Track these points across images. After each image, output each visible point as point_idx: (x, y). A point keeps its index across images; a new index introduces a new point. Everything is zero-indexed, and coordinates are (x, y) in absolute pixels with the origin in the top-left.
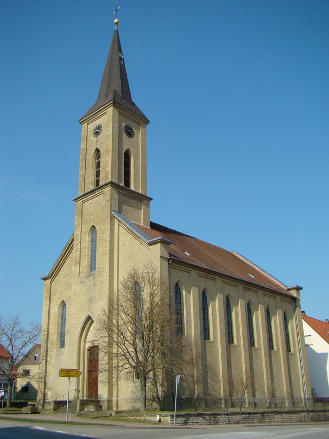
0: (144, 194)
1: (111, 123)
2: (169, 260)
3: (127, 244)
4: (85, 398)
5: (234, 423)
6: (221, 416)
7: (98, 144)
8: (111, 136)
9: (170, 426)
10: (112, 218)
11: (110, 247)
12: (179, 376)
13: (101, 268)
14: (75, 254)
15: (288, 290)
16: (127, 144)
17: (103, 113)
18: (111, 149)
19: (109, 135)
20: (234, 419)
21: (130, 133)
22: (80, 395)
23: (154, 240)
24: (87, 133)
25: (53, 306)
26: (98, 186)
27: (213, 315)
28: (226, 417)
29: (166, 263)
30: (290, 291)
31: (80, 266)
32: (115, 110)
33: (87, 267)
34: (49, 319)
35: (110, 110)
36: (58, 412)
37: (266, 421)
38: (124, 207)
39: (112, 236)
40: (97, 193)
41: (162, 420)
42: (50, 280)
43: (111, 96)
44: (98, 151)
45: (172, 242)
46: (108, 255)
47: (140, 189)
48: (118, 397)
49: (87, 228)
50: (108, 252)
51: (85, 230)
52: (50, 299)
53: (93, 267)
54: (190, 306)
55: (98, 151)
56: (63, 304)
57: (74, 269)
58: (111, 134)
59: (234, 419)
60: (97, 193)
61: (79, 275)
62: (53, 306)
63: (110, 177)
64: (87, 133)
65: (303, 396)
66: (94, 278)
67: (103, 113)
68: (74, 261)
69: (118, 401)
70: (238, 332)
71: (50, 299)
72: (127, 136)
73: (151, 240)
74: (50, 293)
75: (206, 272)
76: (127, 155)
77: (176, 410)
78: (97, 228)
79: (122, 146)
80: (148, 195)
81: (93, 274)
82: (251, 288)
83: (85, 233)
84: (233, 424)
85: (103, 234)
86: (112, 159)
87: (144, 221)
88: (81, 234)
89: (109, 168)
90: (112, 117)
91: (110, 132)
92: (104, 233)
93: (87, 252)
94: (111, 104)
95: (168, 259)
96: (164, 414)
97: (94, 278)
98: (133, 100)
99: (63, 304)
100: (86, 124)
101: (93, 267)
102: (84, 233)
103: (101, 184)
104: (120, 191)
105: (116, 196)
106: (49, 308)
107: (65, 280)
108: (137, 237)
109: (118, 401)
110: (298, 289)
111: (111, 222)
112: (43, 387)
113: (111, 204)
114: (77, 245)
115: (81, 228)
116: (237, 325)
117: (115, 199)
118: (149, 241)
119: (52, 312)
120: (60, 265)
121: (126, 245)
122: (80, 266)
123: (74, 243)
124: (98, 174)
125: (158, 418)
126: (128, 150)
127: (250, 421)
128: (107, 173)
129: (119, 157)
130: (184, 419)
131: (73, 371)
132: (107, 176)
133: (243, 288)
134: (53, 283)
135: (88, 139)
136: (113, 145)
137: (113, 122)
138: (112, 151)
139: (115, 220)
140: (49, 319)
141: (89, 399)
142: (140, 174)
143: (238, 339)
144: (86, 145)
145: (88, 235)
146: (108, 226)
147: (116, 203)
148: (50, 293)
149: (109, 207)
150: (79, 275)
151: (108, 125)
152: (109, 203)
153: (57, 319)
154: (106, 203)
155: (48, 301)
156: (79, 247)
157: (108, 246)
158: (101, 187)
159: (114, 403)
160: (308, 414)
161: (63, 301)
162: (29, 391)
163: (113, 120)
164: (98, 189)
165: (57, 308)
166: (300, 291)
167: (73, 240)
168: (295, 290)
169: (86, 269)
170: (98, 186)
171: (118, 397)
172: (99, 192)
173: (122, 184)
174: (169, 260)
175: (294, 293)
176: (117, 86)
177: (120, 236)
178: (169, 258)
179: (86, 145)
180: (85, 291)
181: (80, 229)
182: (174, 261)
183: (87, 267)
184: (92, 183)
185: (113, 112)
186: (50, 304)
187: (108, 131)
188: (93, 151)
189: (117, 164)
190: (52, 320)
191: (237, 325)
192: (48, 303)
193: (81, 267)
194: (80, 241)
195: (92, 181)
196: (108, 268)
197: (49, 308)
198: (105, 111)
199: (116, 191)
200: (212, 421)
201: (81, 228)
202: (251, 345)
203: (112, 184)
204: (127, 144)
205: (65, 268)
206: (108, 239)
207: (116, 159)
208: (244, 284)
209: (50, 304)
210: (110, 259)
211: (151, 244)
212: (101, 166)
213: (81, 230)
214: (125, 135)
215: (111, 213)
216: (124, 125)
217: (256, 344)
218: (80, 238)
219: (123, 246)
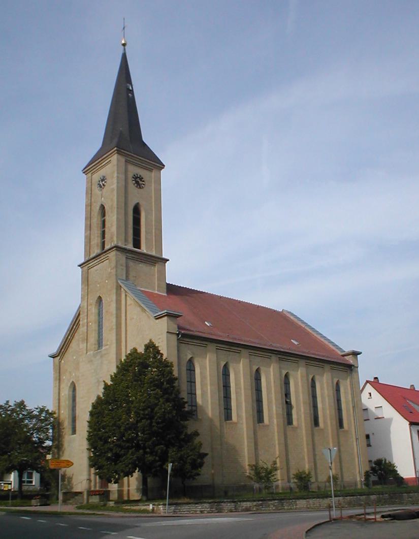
0: (158, 255)
1: (115, 175)
2: (178, 335)
3: (135, 317)
4: (97, 489)
5: (243, 511)
6: (225, 504)
7: (103, 199)
8: (116, 190)
9: (162, 514)
10: (119, 288)
11: (117, 321)
12: (171, 464)
13: (107, 345)
14: (82, 329)
15: (343, 356)
17: (107, 161)
18: (116, 206)
19: (113, 189)
20: (242, 507)
21: (138, 181)
22: (92, 484)
23: (160, 313)
24: (91, 185)
25: (63, 388)
26: (104, 251)
27: (237, 393)
28: (233, 504)
29: (174, 338)
30: (346, 357)
31: (87, 342)
33: (95, 344)
34: (59, 403)
35: (115, 158)
37: (286, 507)
39: (118, 309)
40: (102, 258)
41: (155, 509)
42: (59, 357)
43: (115, 141)
44: (103, 208)
45: (181, 314)
46: (115, 330)
47: (154, 249)
48: (129, 486)
50: (115, 327)
51: (91, 301)
52: (60, 380)
53: (100, 344)
54: (207, 384)
55: (103, 208)
56: (73, 387)
57: (81, 346)
58: (116, 188)
59: (242, 507)
60: (102, 258)
61: (87, 353)
62: (63, 388)
63: (115, 239)
64: (91, 185)
65: (358, 479)
67: (107, 161)
68: (81, 336)
69: (129, 490)
70: (270, 410)
71: (60, 380)
72: (137, 187)
73: (157, 314)
74: (60, 373)
75: (227, 345)
76: (137, 210)
77: (169, 498)
78: (103, 299)
80: (164, 256)
81: (100, 352)
82: (289, 358)
83: (91, 305)
84: (242, 511)
85: (110, 306)
86: (117, 218)
87: (158, 287)
89: (114, 229)
91: (115, 186)
92: (110, 305)
93: (94, 326)
94: (115, 151)
95: (177, 334)
96: (156, 503)
99: (73, 387)
100: (90, 174)
101: (100, 344)
103: (107, 247)
104: (128, 254)
106: (59, 389)
107: (74, 358)
108: (144, 310)
109: (129, 490)
110: (355, 354)
111: (116, 293)
114: (83, 319)
115: (88, 298)
116: (269, 402)
118: (155, 315)
119: (62, 394)
120: (67, 342)
121: (133, 318)
122: (87, 342)
123: (81, 316)
124: (103, 236)
125: (151, 507)
126: (138, 203)
127: (263, 509)
129: (126, 214)
130: (173, 508)
131: (63, 462)
132: (112, 238)
133: (278, 359)
134: (63, 362)
135: (93, 193)
136: (118, 201)
137: (118, 173)
138: (117, 208)
139: (122, 289)
140: (59, 403)
141: (102, 489)
142: (154, 231)
143: (270, 417)
144: (91, 200)
145: (96, 305)
146: (114, 297)
147: (122, 269)
148: (60, 373)
149: (115, 275)
150: (87, 353)
151: (113, 177)
152: (115, 270)
153: (67, 403)
154: (111, 270)
155: (58, 382)
156: (86, 321)
157: (114, 320)
158: (105, 252)
159: (125, 493)
160: (343, 499)
161: (73, 382)
163: (117, 170)
164: (103, 253)
165: (68, 390)
166: (358, 356)
167: (79, 314)
168: (351, 356)
169: (94, 346)
170: (104, 251)
171: (129, 486)
172: (104, 257)
173: (130, 246)
174: (178, 335)
175: (350, 360)
176: (123, 127)
177: (128, 307)
178: (177, 332)
179: (91, 200)
180: (93, 371)
181: (86, 300)
182: (184, 336)
183: (95, 344)
184: (98, 245)
185: (118, 160)
186: (59, 386)
187: (113, 184)
188: (98, 208)
189: (123, 224)
190: (62, 404)
191: (269, 402)
192: (58, 385)
193: (88, 344)
194: (86, 314)
196: (114, 345)
197: (59, 389)
198: (109, 160)
200: (214, 509)
201: (88, 298)
204: (135, 196)
205: (74, 345)
206: (114, 312)
207: (122, 217)
208: (280, 354)
209: (59, 386)
210: (117, 335)
211: (157, 318)
212: (106, 226)
213: (87, 302)
215: (117, 282)
216: (130, 175)
217: (295, 423)
219: (131, 319)
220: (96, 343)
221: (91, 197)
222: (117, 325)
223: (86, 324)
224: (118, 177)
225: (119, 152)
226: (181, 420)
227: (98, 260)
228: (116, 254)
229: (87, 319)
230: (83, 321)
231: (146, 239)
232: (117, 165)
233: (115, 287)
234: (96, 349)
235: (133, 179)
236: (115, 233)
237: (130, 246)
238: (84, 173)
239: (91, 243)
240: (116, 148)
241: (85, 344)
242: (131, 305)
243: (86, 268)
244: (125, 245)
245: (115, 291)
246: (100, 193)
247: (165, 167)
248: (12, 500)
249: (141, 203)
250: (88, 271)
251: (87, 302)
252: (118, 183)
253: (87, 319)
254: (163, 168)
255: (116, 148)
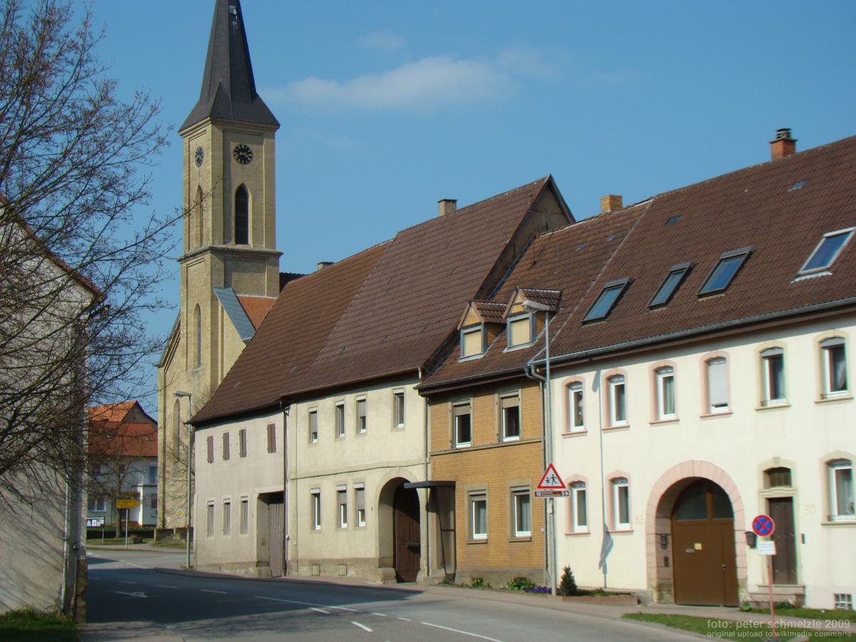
0: (270, 250)
16: (239, 174)
21: (244, 156)
31: (187, 358)
32: (216, 129)
35: (209, 128)
36: (764, 476)
38: (235, 276)
46: (210, 349)
49: (192, 307)
50: (210, 345)
61: (187, 370)
66: (199, 377)
72: (241, 162)
76: (242, 193)
79: (231, 184)
88: (187, 312)
90: (210, 142)
94: (208, 121)
97: (199, 377)
98: (259, 91)
102: (191, 312)
105: (221, 265)
112: (166, 504)
113: (212, 278)
115: (187, 304)
117: (218, 270)
122: (187, 358)
128: (208, 228)
134: (168, 373)
137: (213, 151)
147: (219, 275)
150: (187, 370)
162: (672, 383)
169: (193, 363)
181: (186, 306)
185: (213, 133)
188: (196, 189)
193: (189, 359)
195: (196, 235)
199: (219, 259)
201: (187, 304)
202: (338, 527)
203: (213, 250)
204: (239, 174)
214: (236, 163)
215: (212, 292)
216: (233, 146)
218: (185, 318)
220: (196, 359)
221: (189, 170)
222: (212, 343)
223: (185, 335)
224: (213, 156)
225: (213, 122)
226: (91, 618)
227: (196, 260)
228: (211, 258)
229: (187, 329)
230: (183, 331)
231: (253, 228)
232: (212, 139)
233: (210, 298)
234: (196, 366)
235: (236, 153)
236: (211, 229)
237: (232, 245)
238: (181, 135)
239: (191, 233)
240: (209, 118)
241: (185, 360)
242: (227, 319)
243: (185, 265)
244: (224, 243)
245: (209, 302)
246: (197, 169)
247: (281, 127)
248: (105, 538)
249: (246, 184)
250: (187, 270)
251: (187, 307)
252: (213, 164)
253: (187, 329)
254: (278, 128)
255: (209, 118)
